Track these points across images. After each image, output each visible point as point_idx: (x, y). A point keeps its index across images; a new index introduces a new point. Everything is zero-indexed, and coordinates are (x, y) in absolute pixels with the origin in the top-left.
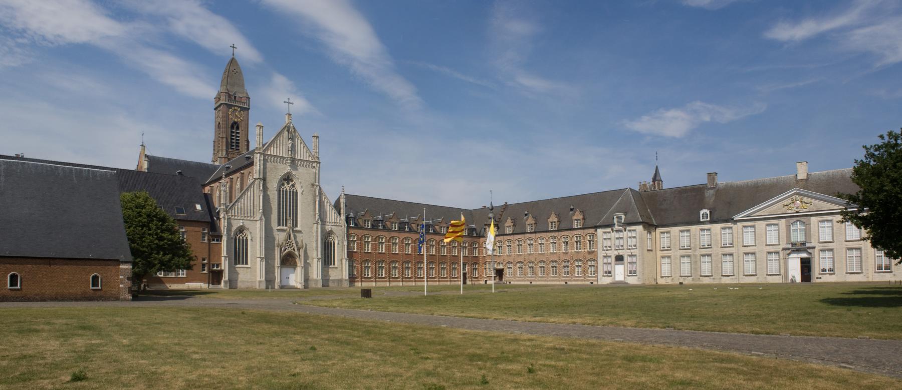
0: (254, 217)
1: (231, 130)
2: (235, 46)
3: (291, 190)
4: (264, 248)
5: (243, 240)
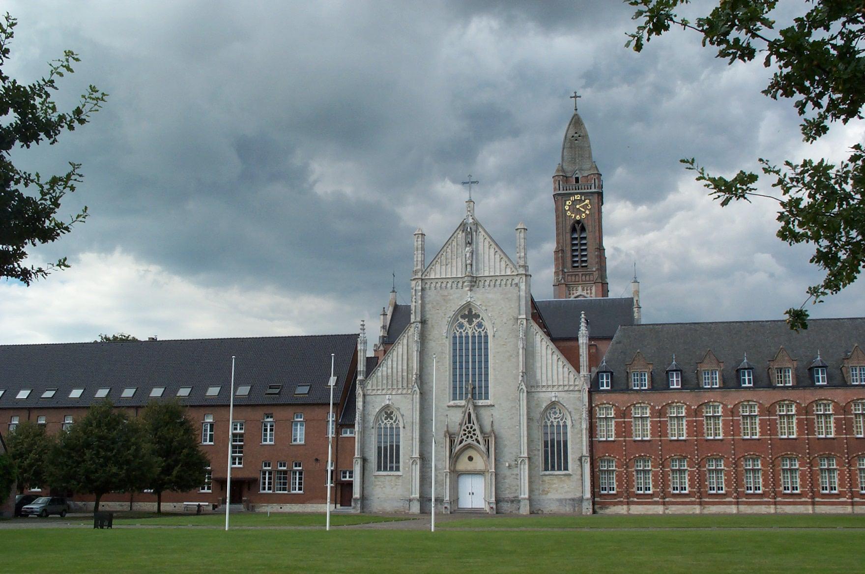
0: (785, 383)
4: (418, 440)
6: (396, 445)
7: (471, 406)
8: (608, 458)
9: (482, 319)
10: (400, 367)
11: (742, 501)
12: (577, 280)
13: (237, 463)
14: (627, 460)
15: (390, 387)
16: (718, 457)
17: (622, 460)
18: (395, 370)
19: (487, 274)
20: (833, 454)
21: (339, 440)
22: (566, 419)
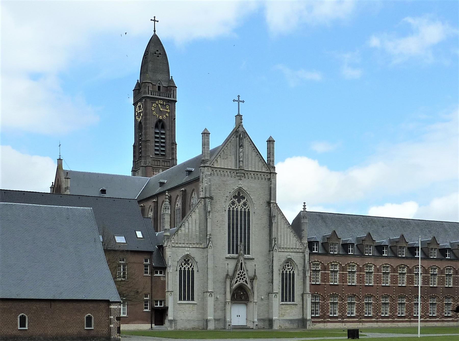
2: (156, 20)
3: (231, 209)
5: (189, 271)
11: (380, 320)
21: (153, 278)
22: (193, 267)
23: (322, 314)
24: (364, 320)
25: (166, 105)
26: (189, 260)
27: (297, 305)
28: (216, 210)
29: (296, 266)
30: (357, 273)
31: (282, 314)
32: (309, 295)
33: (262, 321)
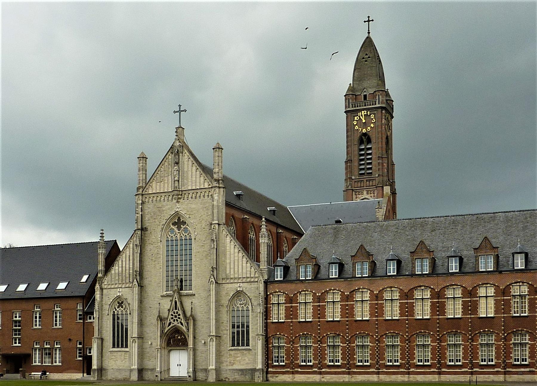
1: (358, 147)
2: (370, 19)
6: (125, 328)
7: (176, 295)
8: (280, 336)
9: (187, 225)
10: (127, 266)
12: (362, 185)
13: (17, 343)
14: (294, 338)
15: (120, 282)
16: (365, 334)
17: (290, 338)
18: (124, 269)
19: (190, 188)
20: (459, 331)
21: (85, 324)
23: (288, 362)
24: (355, 370)
25: (370, 115)
26: (123, 302)
27: (251, 350)
28: (150, 242)
29: (249, 300)
30: (341, 303)
31: (230, 362)
32: (95, 340)
33: (204, 371)
